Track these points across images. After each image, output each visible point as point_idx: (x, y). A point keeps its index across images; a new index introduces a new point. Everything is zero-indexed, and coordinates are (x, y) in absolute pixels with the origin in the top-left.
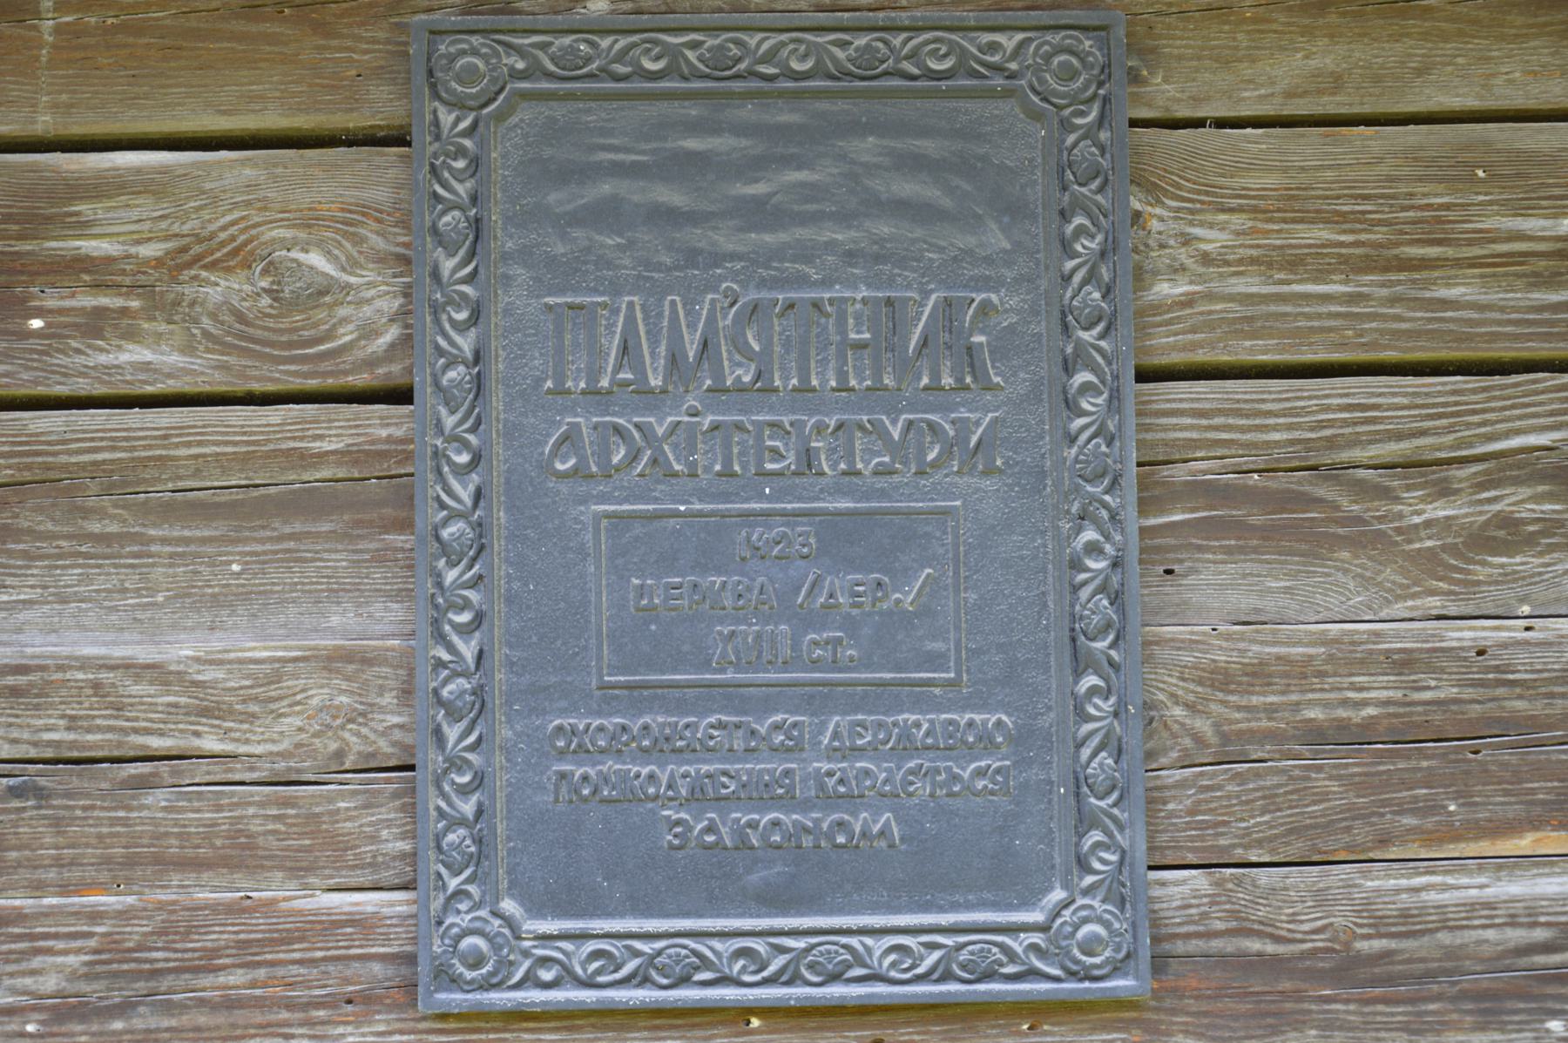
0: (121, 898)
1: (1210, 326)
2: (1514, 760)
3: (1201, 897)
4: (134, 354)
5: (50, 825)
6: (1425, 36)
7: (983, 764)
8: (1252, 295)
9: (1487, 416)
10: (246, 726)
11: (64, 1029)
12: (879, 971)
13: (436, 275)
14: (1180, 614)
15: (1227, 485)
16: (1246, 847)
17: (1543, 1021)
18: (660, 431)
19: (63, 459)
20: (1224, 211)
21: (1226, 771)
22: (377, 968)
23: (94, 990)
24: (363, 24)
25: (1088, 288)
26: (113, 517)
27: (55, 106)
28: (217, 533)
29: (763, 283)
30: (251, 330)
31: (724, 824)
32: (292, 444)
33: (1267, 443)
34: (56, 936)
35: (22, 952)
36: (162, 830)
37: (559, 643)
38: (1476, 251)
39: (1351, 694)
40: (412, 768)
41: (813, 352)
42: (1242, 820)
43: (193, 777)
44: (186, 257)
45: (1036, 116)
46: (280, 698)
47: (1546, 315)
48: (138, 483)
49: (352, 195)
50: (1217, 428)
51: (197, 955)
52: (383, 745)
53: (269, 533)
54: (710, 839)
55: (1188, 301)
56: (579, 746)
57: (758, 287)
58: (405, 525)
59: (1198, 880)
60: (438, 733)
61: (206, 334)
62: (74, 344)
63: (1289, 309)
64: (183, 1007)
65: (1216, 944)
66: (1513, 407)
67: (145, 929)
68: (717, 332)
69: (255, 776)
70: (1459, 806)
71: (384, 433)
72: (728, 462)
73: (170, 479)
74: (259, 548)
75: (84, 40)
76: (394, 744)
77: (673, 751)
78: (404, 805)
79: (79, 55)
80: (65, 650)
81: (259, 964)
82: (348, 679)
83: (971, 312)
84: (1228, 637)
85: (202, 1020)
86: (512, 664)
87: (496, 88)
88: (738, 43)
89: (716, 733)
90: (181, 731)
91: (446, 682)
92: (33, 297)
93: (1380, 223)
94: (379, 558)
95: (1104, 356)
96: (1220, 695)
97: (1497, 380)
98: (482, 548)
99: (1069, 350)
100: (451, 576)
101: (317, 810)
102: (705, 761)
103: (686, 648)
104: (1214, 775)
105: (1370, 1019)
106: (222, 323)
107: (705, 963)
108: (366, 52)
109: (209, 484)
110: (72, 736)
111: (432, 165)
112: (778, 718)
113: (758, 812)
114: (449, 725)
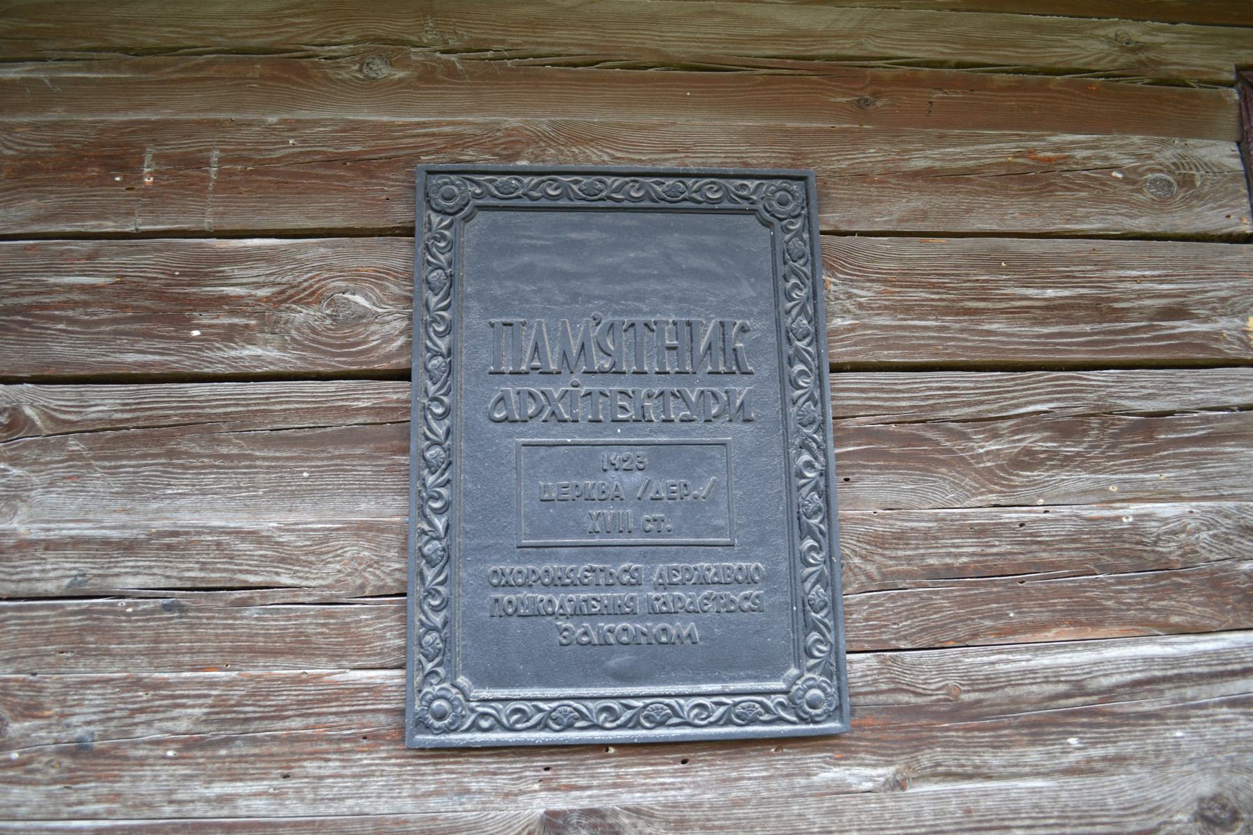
0: (229, 673)
1: (864, 342)
2: (1043, 586)
3: (873, 670)
4: (250, 351)
5: (187, 628)
6: (969, 193)
7: (747, 592)
8: (886, 326)
9: (1015, 394)
10: (306, 569)
11: (190, 754)
12: (688, 720)
13: (427, 307)
14: (854, 502)
15: (878, 431)
16: (897, 640)
17: (1066, 739)
18: (556, 396)
19: (208, 411)
20: (869, 281)
21: (885, 595)
22: (382, 718)
23: (210, 732)
24: (391, 171)
25: (800, 318)
26: (236, 445)
27: (216, 213)
28: (296, 454)
29: (615, 313)
30: (319, 338)
31: (594, 630)
32: (341, 403)
33: (898, 407)
34: (188, 696)
35: (167, 706)
36: (254, 631)
37: (495, 520)
38: (1004, 305)
39: (953, 550)
40: (404, 595)
41: (645, 352)
42: (895, 624)
43: (274, 599)
44: (284, 296)
45: (767, 224)
46: (328, 552)
47: (1042, 340)
48: (250, 425)
49: (380, 263)
50: (870, 399)
51: (272, 709)
52: (389, 581)
53: (326, 455)
54: (585, 639)
55: (852, 329)
56: (507, 582)
57: (613, 315)
58: (405, 451)
59: (870, 660)
60: (421, 575)
61: (293, 339)
62: (217, 345)
63: (907, 334)
64: (262, 741)
65: (882, 698)
66: (1028, 389)
67: (242, 693)
68: (589, 340)
69: (311, 599)
70: (1016, 613)
71: (395, 397)
72: (596, 413)
73: (269, 423)
74: (320, 463)
75: (234, 178)
76: (396, 580)
77: (563, 585)
78: (401, 617)
79: (231, 185)
80: (201, 523)
81: (311, 715)
82: (369, 541)
83: (735, 329)
84: (882, 517)
85: (275, 749)
86: (467, 533)
87: (464, 203)
88: (600, 181)
89: (589, 574)
90: (268, 572)
91: (427, 543)
92: (194, 318)
93: (954, 289)
94: (391, 469)
95: (811, 355)
96: (880, 551)
97: (1019, 375)
98: (450, 463)
99: (791, 352)
100: (431, 479)
101: (348, 620)
102: (582, 592)
103: (571, 523)
104: (879, 597)
105: (970, 740)
106: (303, 333)
107: (583, 716)
108: (392, 186)
109: (292, 426)
110: (202, 575)
111: (427, 245)
112: (626, 565)
113: (614, 622)
114: (428, 569)
